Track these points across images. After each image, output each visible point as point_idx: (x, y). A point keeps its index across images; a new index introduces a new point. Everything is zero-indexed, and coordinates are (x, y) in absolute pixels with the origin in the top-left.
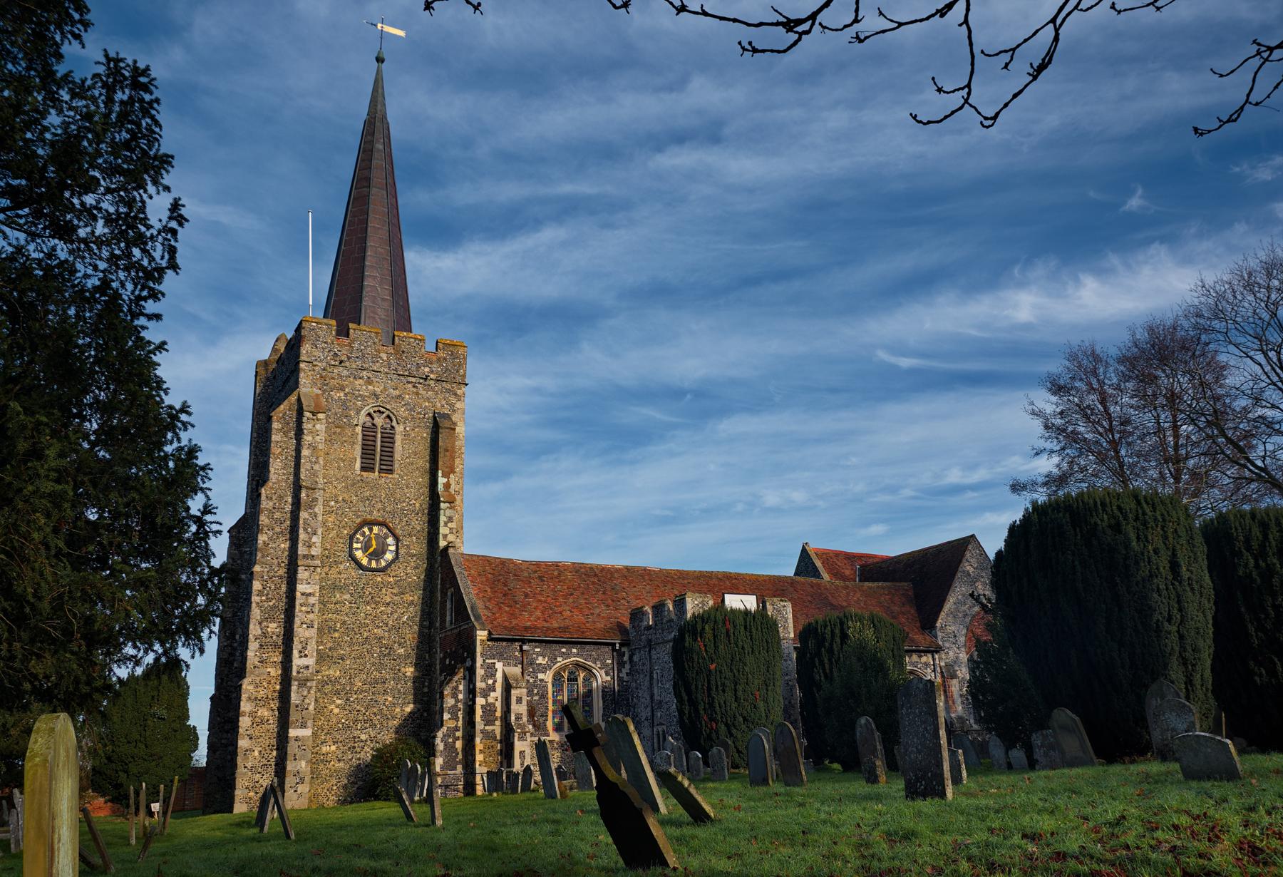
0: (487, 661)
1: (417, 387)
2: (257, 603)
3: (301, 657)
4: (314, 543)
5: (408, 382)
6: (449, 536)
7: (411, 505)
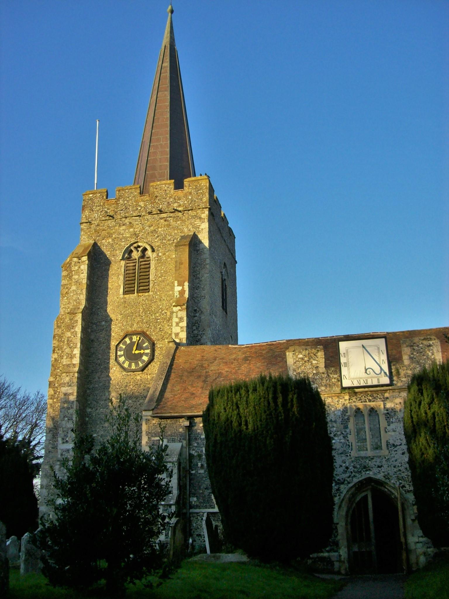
0: (153, 439)
1: (168, 221)
2: (51, 405)
3: (63, 443)
4: (75, 354)
5: (161, 219)
6: (180, 334)
7: (163, 314)
